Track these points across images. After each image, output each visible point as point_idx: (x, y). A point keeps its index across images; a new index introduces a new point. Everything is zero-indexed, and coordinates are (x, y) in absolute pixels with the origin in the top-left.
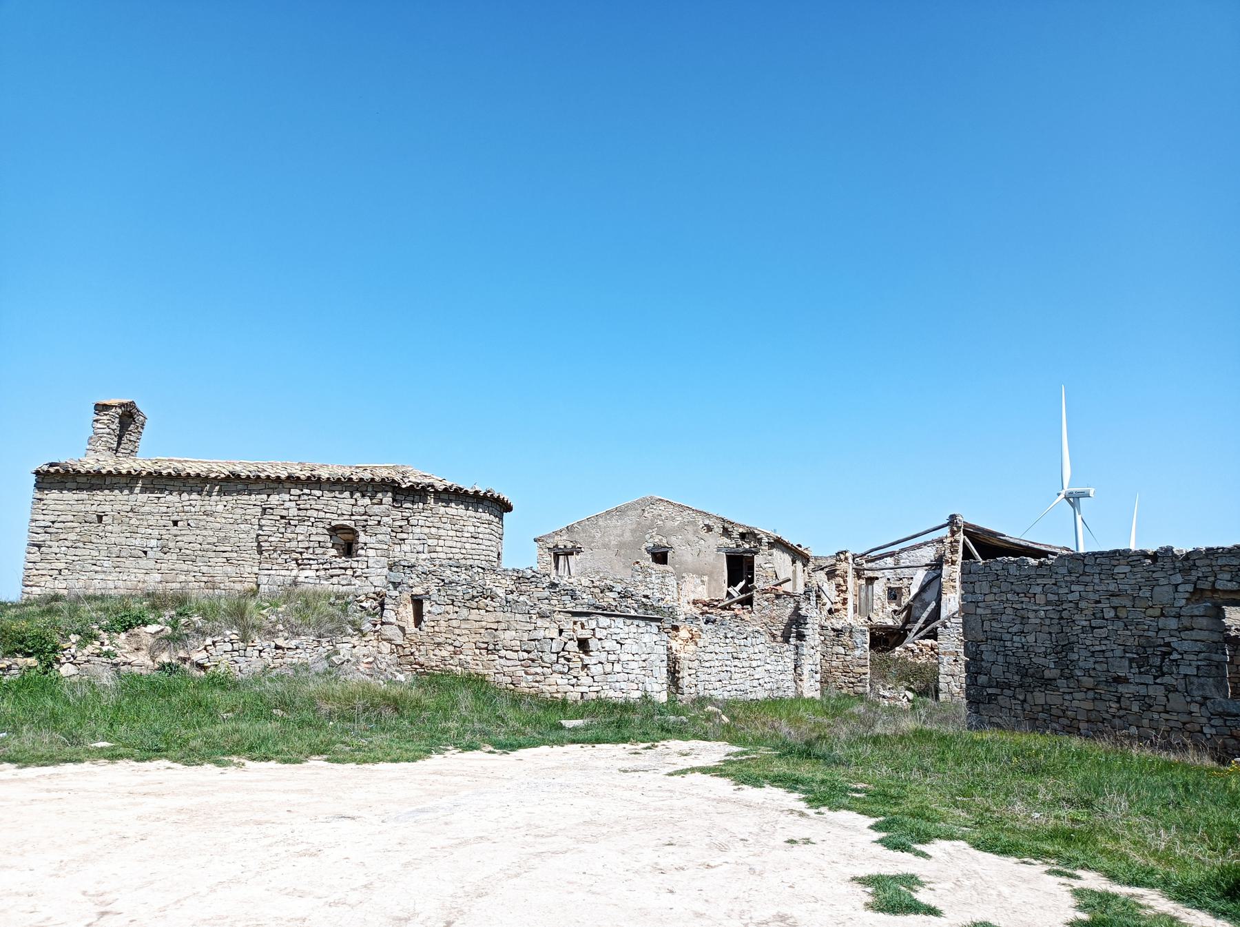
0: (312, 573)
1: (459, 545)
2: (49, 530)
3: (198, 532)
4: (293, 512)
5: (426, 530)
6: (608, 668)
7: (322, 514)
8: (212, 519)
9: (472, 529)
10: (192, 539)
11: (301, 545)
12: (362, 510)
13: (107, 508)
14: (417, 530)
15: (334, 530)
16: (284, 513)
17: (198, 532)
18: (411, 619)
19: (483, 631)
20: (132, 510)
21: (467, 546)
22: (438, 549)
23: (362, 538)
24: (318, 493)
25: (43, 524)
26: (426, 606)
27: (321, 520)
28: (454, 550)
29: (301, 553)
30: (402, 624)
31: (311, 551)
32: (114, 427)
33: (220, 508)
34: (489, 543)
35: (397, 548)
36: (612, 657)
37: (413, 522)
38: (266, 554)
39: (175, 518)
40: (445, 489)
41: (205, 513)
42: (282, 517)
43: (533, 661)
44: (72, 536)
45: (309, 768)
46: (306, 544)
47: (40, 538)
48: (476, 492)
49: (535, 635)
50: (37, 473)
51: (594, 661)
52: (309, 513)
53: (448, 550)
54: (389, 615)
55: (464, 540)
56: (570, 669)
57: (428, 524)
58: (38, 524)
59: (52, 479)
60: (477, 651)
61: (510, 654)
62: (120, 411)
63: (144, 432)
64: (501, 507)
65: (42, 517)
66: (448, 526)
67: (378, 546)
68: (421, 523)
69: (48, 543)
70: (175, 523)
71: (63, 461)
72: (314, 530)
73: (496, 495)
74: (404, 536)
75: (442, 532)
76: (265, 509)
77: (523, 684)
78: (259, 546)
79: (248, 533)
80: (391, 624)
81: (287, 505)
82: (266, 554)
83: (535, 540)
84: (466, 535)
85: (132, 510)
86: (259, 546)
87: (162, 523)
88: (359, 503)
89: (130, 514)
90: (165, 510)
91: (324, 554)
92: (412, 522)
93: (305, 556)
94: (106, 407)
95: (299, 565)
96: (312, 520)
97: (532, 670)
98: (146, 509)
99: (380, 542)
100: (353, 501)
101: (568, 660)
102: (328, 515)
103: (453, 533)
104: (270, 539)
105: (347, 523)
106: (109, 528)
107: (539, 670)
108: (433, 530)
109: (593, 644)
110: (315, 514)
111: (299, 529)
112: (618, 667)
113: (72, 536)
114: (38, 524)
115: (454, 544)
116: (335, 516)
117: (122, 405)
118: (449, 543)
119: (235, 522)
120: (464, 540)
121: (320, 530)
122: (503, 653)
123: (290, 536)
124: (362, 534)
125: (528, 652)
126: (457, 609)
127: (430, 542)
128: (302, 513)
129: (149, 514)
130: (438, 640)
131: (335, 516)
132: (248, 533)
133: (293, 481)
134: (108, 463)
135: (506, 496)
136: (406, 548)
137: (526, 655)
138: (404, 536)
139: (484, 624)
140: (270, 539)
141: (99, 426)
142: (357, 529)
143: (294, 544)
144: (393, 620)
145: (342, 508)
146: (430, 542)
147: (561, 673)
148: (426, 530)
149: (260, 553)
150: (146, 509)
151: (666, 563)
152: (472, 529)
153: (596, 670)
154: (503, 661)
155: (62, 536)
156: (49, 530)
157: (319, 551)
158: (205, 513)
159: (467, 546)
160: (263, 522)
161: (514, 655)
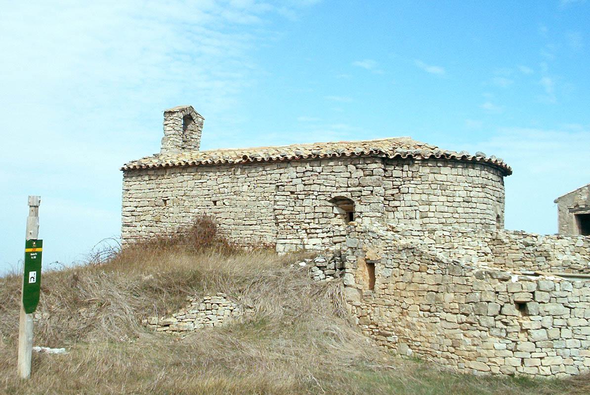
0: (319, 241)
1: (451, 210)
2: (134, 213)
3: (231, 209)
4: (300, 187)
6: (554, 333)
7: (323, 188)
8: (240, 198)
9: (463, 193)
10: (227, 215)
11: (308, 216)
12: (356, 182)
13: (169, 194)
14: (408, 197)
16: (293, 189)
17: (231, 209)
19: (425, 294)
22: (430, 214)
23: (358, 208)
24: (319, 169)
26: (378, 267)
27: (322, 193)
28: (446, 215)
29: (309, 223)
30: (360, 287)
32: (178, 128)
33: (245, 188)
34: (484, 207)
35: (391, 215)
37: (404, 190)
38: (281, 225)
39: (214, 199)
40: (432, 157)
41: (235, 193)
42: (292, 193)
43: (471, 324)
44: (149, 218)
45: (509, 371)
47: (129, 220)
49: (471, 297)
50: (123, 169)
52: (313, 187)
54: (349, 278)
55: (455, 204)
56: (507, 333)
59: (132, 172)
60: (421, 313)
61: (449, 317)
63: (203, 130)
64: (503, 171)
66: (439, 192)
67: (371, 214)
69: (134, 223)
70: (215, 202)
71: (137, 159)
72: (317, 203)
74: (397, 203)
75: (432, 198)
76: (278, 186)
77: (463, 347)
78: (276, 219)
79: (267, 207)
80: (351, 286)
81: (295, 181)
84: (457, 199)
86: (276, 219)
87: (205, 203)
88: (353, 176)
89: (184, 198)
90: (206, 192)
92: (403, 190)
93: (312, 225)
95: (308, 234)
96: (316, 193)
97: (470, 333)
99: (373, 210)
100: (348, 175)
101: (506, 324)
103: (444, 199)
104: (284, 212)
105: (344, 194)
106: (171, 209)
108: (424, 197)
109: (531, 307)
110: (317, 188)
113: (149, 218)
115: (446, 209)
117: (182, 110)
118: (442, 209)
120: (455, 204)
121: (323, 203)
122: (443, 315)
123: (299, 209)
125: (467, 315)
126: (403, 272)
128: (307, 188)
129: (196, 196)
130: (388, 302)
131: (334, 189)
132: (267, 207)
133: (299, 160)
134: (174, 157)
135: (508, 163)
136: (399, 215)
137: (464, 318)
138: (397, 203)
139: (426, 286)
140: (284, 212)
141: (168, 129)
142: (353, 199)
143: (302, 216)
144: (352, 283)
145: (338, 181)
146: (421, 208)
147: (500, 337)
148: (417, 197)
149: (277, 224)
152: (463, 193)
154: (444, 324)
155: (142, 218)
156: (134, 213)
157: (323, 221)
158: (235, 193)
159: (460, 210)
160: (277, 198)
161: (454, 318)
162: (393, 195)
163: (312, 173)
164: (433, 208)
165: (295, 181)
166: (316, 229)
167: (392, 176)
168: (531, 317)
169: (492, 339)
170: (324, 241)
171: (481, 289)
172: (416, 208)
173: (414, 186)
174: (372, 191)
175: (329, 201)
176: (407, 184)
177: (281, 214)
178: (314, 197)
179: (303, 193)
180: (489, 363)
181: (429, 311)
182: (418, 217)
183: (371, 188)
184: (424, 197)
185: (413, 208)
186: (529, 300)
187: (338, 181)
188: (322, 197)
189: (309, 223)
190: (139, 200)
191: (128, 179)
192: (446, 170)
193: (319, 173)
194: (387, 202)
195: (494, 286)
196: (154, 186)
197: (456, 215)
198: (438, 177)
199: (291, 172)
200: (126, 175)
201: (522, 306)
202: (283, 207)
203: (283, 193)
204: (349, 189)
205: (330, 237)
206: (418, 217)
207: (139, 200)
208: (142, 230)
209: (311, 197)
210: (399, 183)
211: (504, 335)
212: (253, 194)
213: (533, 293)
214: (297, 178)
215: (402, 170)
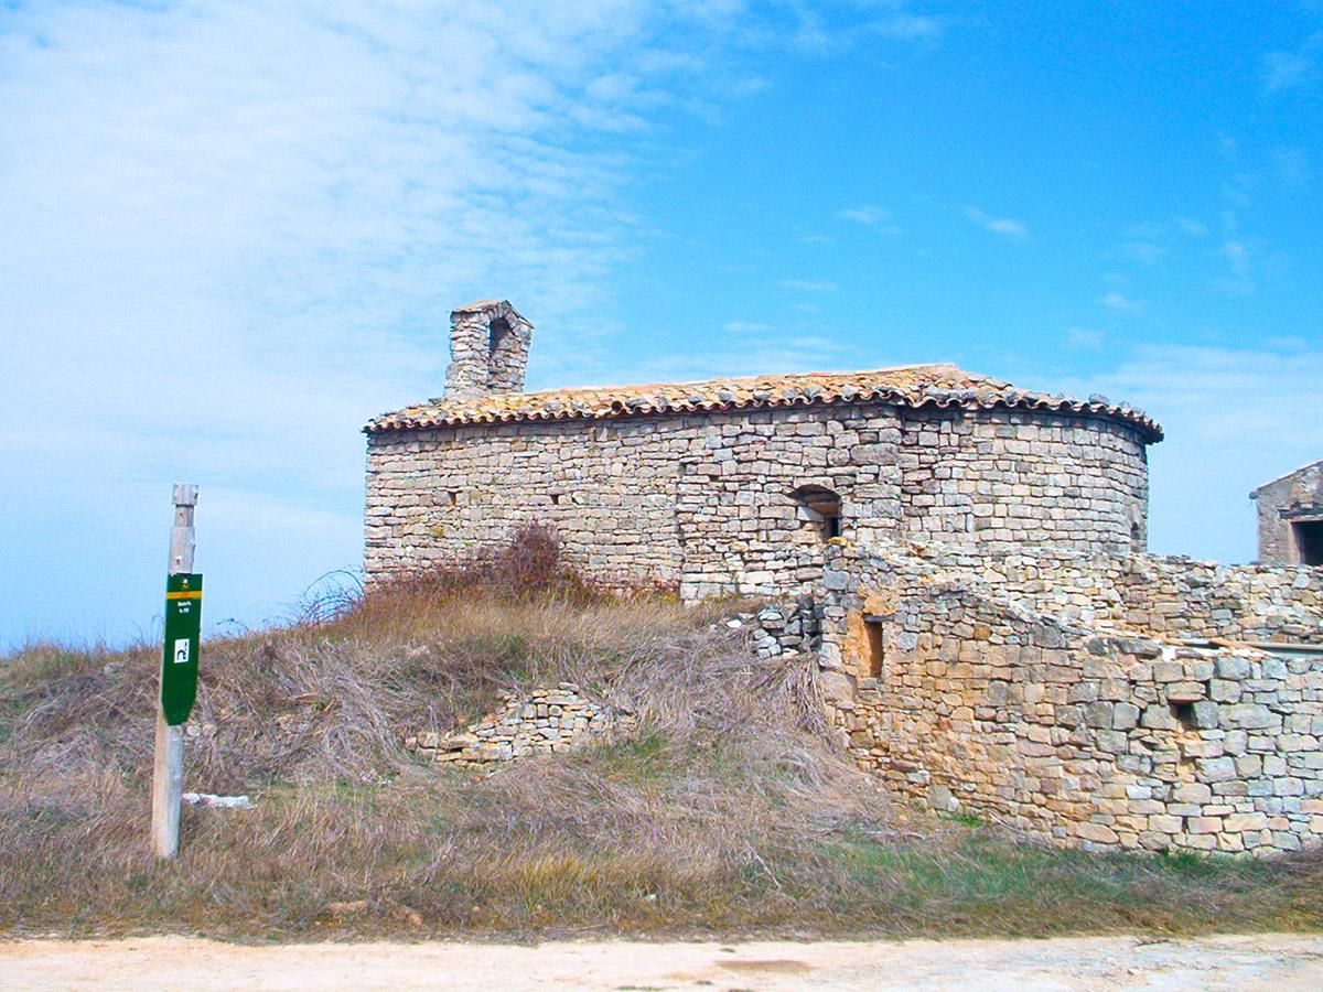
0: (767, 577)
1: (1038, 513)
2: (390, 520)
3: (589, 512)
4: (730, 466)
5: (969, 487)
7: (776, 469)
8: (607, 488)
9: (1064, 480)
10: (581, 524)
12: (845, 455)
13: (460, 480)
15: (803, 495)
16: (714, 470)
17: (589, 512)
18: (866, 665)
19: (986, 684)
20: (493, 482)
21: (1056, 513)
22: (996, 522)
23: (849, 509)
24: (767, 430)
25: (381, 510)
26: (888, 629)
28: (1027, 523)
30: (850, 670)
31: (763, 535)
32: (479, 346)
33: (617, 468)
34: (1107, 506)
35: (915, 523)
36: (1258, 743)
38: (691, 544)
39: (553, 490)
42: (713, 478)
43: (1080, 746)
46: (753, 525)
47: (379, 533)
48: (1065, 405)
51: (1210, 750)
52: (755, 467)
53: (1015, 524)
55: (1048, 502)
56: (1154, 765)
57: (971, 475)
58: (376, 511)
59: (385, 435)
60: (978, 725)
62: (486, 319)
64: (1144, 434)
65: (378, 501)
67: (876, 521)
68: (957, 473)
70: (555, 498)
72: (765, 499)
73: (1113, 407)
74: (927, 499)
77: (1063, 795)
81: (719, 454)
82: (691, 544)
83: (1253, 496)
84: (1052, 492)
85: (493, 482)
86: (680, 531)
87: (535, 499)
89: (492, 488)
90: (537, 477)
91: (786, 541)
92: (939, 473)
93: (754, 545)
94: (466, 314)
95: (746, 562)
96: (761, 479)
97: (1078, 765)
98: (513, 478)
99: (879, 514)
100: (828, 441)
101: (1151, 746)
102: (787, 470)
103: (1025, 490)
104: (696, 518)
105: (819, 481)
106: (466, 512)
107: (1091, 766)
108: (984, 487)
109: (1202, 712)
110: (763, 467)
111: (742, 498)
112: (1274, 765)
114: (376, 511)
115: (1029, 511)
116: (800, 471)
117: (488, 309)
118: (1020, 511)
119: (642, 492)
121: (775, 499)
122: (1023, 728)
123: (728, 511)
124: (846, 500)
125: (1071, 728)
126: (940, 640)
127: (978, 509)
129: (516, 485)
131: (800, 471)
133: (728, 411)
136: (929, 523)
137: (1065, 734)
138: (927, 499)
139: (987, 669)
140: (696, 518)
144: (836, 662)
145: (810, 452)
146: (978, 509)
148: (969, 487)
149: (683, 542)
150: (513, 478)
151: (201, 575)
152: (1064, 480)
153: (1212, 768)
155: (407, 529)
156: (390, 520)
157: (776, 535)
158: (596, 479)
159: (1056, 513)
160: (683, 488)
161: (1045, 735)
162: (919, 483)
163: (755, 438)
164: (1001, 509)
165: (719, 454)
166: (761, 551)
167: (917, 444)
168: (1203, 733)
169: (1122, 777)
170: (778, 576)
171: (1099, 674)
172: (967, 509)
173: (963, 464)
174: (877, 475)
175: (789, 495)
176: (949, 460)
177: (690, 522)
178: (758, 487)
179: (735, 478)
180: (1118, 828)
181: (994, 720)
182: (971, 526)
183: (875, 469)
184: (984, 487)
185: (961, 510)
186: (1199, 697)
187: (810, 452)
188: (776, 488)
189: (747, 541)
190: (401, 493)
191: (378, 450)
192: (1028, 432)
193: (769, 438)
194: (908, 498)
195: (1126, 669)
196: (431, 464)
197: (1050, 525)
198: (1013, 446)
199: (711, 435)
200: (373, 442)
201: (1183, 710)
202: (694, 508)
203: (695, 479)
204: (831, 471)
205: (790, 569)
206: (971, 526)
207: (401, 493)
208: (407, 554)
209: (752, 486)
210: (932, 459)
211: (1147, 769)
212: (634, 481)
213: (1207, 683)
214: (723, 447)
215: (939, 432)
